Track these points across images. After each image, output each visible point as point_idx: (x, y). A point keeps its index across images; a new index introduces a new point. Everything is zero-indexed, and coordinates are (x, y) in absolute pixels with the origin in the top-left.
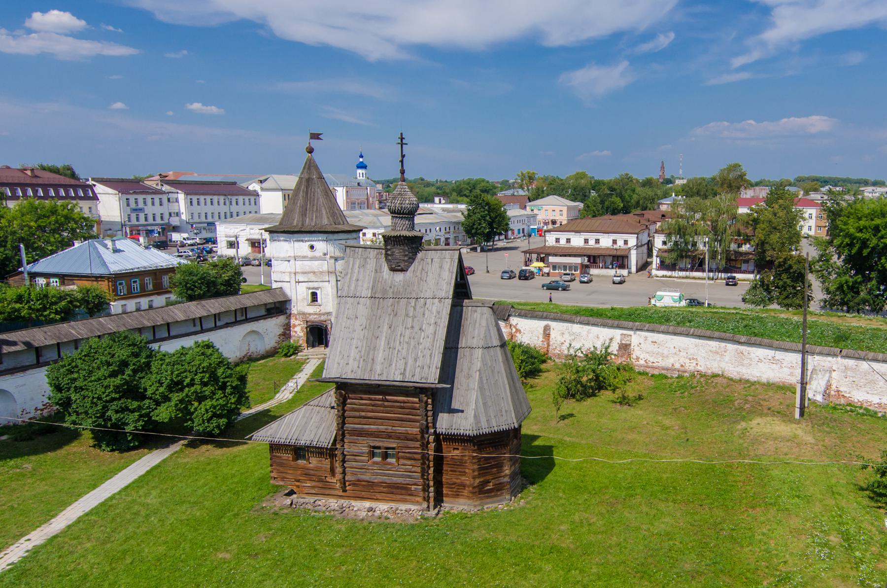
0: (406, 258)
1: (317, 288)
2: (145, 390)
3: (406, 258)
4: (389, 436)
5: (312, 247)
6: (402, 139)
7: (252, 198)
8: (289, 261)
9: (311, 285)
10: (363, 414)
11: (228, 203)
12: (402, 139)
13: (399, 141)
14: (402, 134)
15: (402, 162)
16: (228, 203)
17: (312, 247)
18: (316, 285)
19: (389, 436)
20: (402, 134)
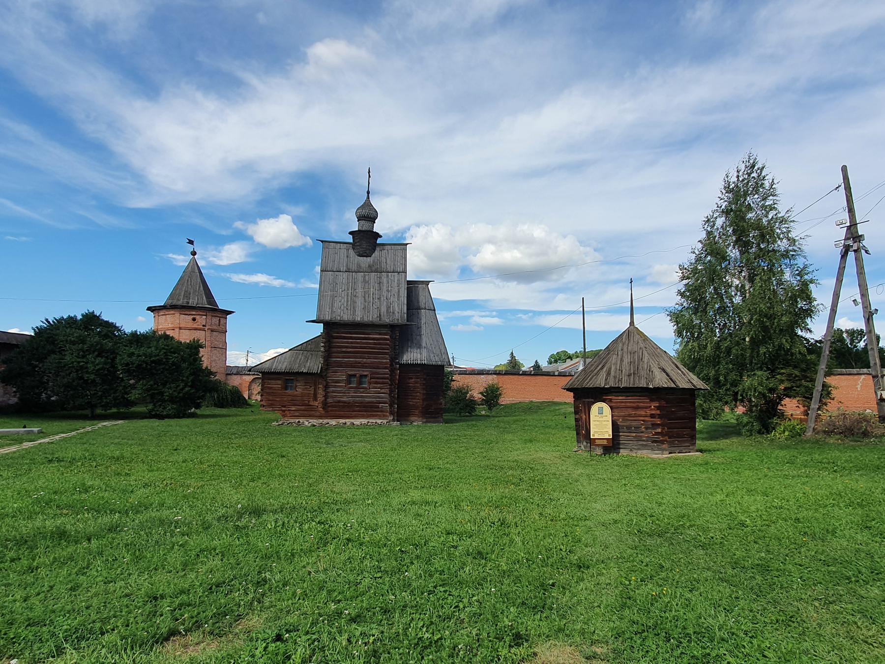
0: (370, 248)
2: (423, 394)
3: (370, 248)
4: (364, 366)
5: (194, 319)
10: (344, 350)
17: (194, 319)
19: (364, 366)
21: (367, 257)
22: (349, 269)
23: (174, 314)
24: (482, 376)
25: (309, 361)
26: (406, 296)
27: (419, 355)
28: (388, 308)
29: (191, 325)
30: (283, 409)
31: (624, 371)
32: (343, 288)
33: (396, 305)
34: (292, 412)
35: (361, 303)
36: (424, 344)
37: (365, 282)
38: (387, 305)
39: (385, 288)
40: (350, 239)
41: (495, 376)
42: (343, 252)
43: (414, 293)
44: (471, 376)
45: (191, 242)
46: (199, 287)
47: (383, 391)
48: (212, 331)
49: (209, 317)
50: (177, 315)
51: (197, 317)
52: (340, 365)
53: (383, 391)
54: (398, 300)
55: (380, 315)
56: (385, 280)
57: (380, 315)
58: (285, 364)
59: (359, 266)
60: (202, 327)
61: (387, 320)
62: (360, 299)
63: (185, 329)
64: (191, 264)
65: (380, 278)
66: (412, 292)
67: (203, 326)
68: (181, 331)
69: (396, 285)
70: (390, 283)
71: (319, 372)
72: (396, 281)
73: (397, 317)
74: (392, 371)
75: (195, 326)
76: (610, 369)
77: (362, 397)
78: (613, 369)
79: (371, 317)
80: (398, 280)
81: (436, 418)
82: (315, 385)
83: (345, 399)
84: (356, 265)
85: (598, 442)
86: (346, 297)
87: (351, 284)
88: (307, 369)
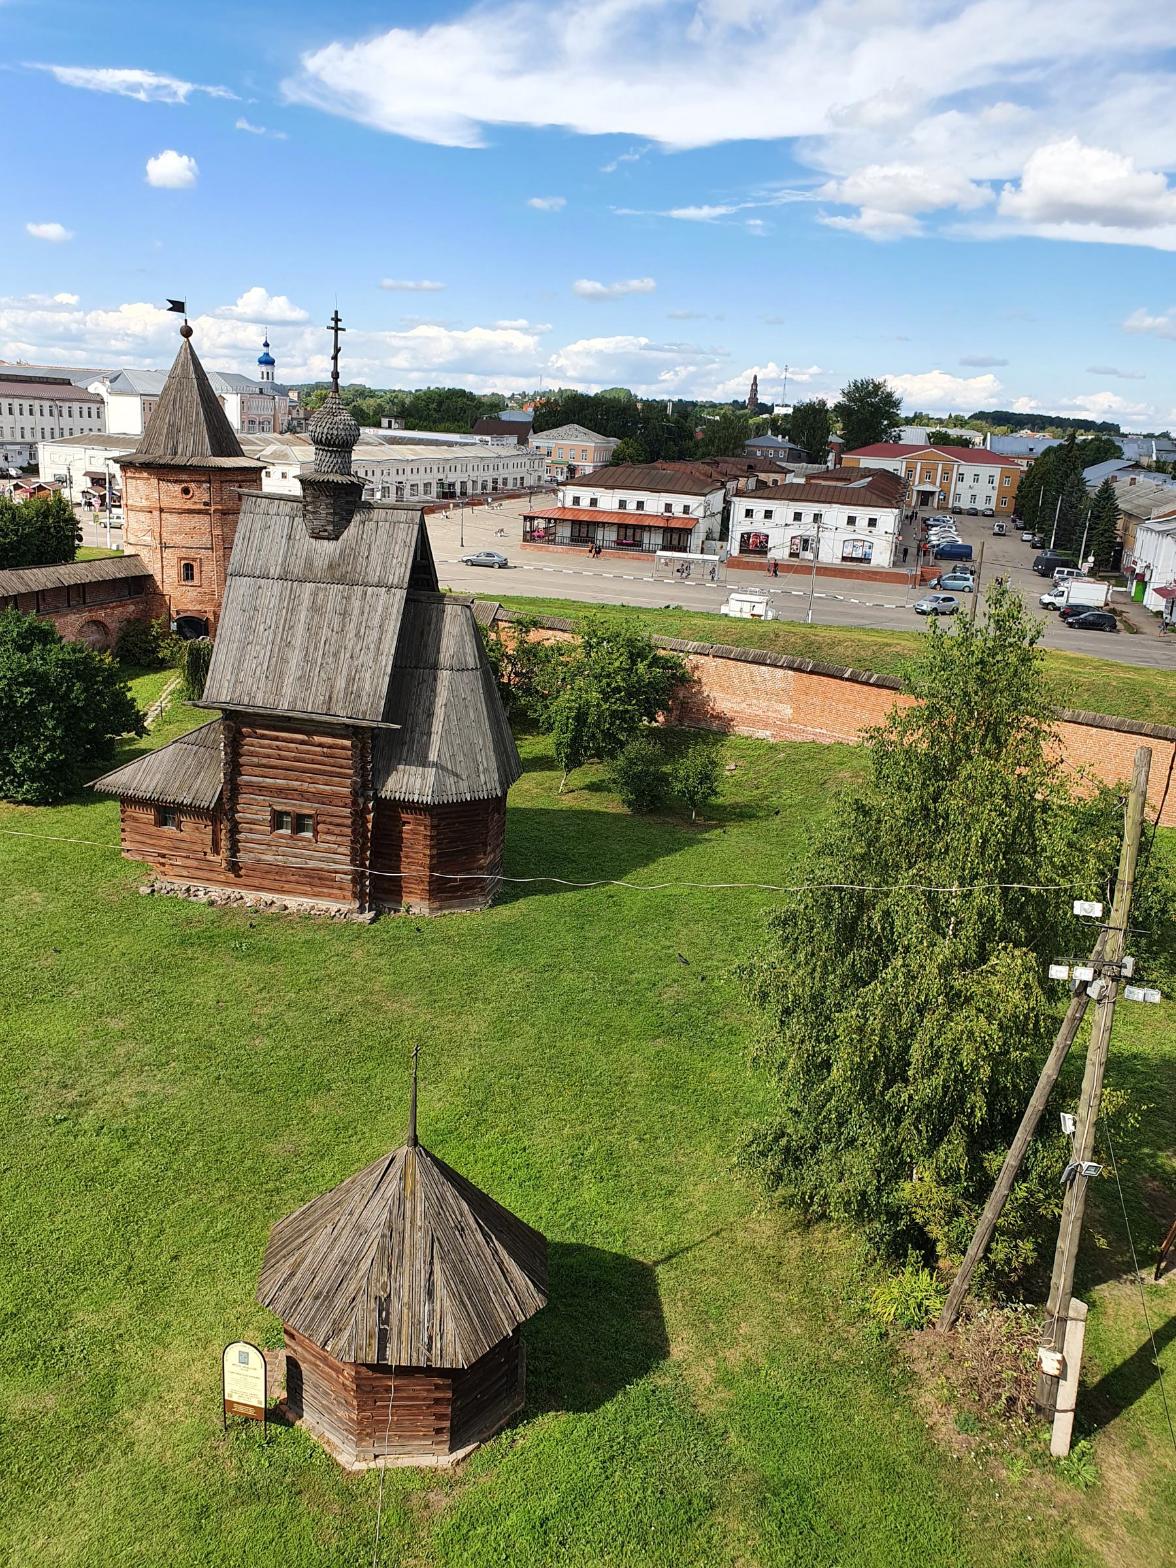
1: (194, 560)
4: (304, 795)
6: (337, 320)
7: (94, 407)
8: (151, 512)
9: (182, 553)
11: (55, 412)
12: (337, 320)
13: (333, 324)
14: (336, 312)
15: (335, 358)
16: (55, 412)
18: (192, 553)
19: (304, 795)
20: (336, 312)
21: (329, 539)
22: (286, 572)
23: (149, 479)
24: (763, 668)
25: (202, 774)
26: (393, 652)
27: (419, 781)
28: (350, 680)
29: (180, 502)
30: (162, 860)
31: (317, 1279)
32: (268, 621)
33: (368, 676)
34: (176, 869)
35: (298, 665)
36: (433, 757)
37: (316, 608)
38: (349, 674)
39: (351, 630)
40: (296, 490)
41: (791, 672)
42: (280, 525)
43: (433, 626)
44: (739, 663)
45: (178, 307)
46: (197, 414)
47: (341, 850)
48: (225, 514)
49: (217, 485)
50: (154, 481)
51: (192, 486)
52: (260, 789)
53: (341, 850)
54: (375, 660)
55: (330, 697)
56: (356, 604)
57: (330, 697)
58: (158, 776)
59: (309, 563)
60: (203, 507)
61: (342, 714)
62: (296, 652)
63: (171, 511)
64: (182, 359)
65: (348, 599)
66: (430, 624)
67: (206, 504)
68: (164, 515)
69: (376, 621)
70: (366, 615)
71: (212, 805)
72: (380, 609)
73: (363, 708)
74: (359, 815)
75: (189, 505)
76: (304, 1259)
77: (302, 857)
78: (308, 1260)
79: (311, 704)
80: (385, 608)
81: (468, 896)
82: (214, 824)
83: (269, 858)
84: (303, 561)
85: (237, 1408)
86: (269, 646)
87: (284, 611)
88: (192, 796)
